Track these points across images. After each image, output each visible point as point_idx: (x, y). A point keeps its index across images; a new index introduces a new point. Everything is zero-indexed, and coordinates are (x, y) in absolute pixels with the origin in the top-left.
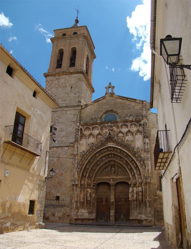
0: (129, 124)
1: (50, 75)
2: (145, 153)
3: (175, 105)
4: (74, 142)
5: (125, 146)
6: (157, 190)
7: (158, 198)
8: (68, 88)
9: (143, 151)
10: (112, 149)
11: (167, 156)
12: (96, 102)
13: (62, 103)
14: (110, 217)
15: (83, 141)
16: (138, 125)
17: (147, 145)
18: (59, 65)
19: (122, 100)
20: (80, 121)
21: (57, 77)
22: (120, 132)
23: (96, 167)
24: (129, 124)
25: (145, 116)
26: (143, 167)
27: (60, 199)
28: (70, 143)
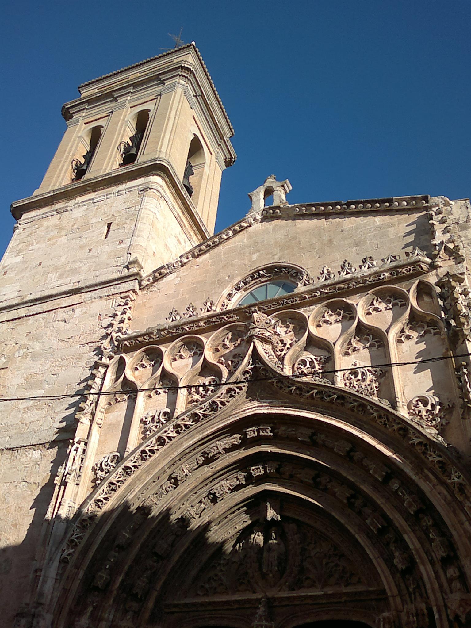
13: (59, 283)
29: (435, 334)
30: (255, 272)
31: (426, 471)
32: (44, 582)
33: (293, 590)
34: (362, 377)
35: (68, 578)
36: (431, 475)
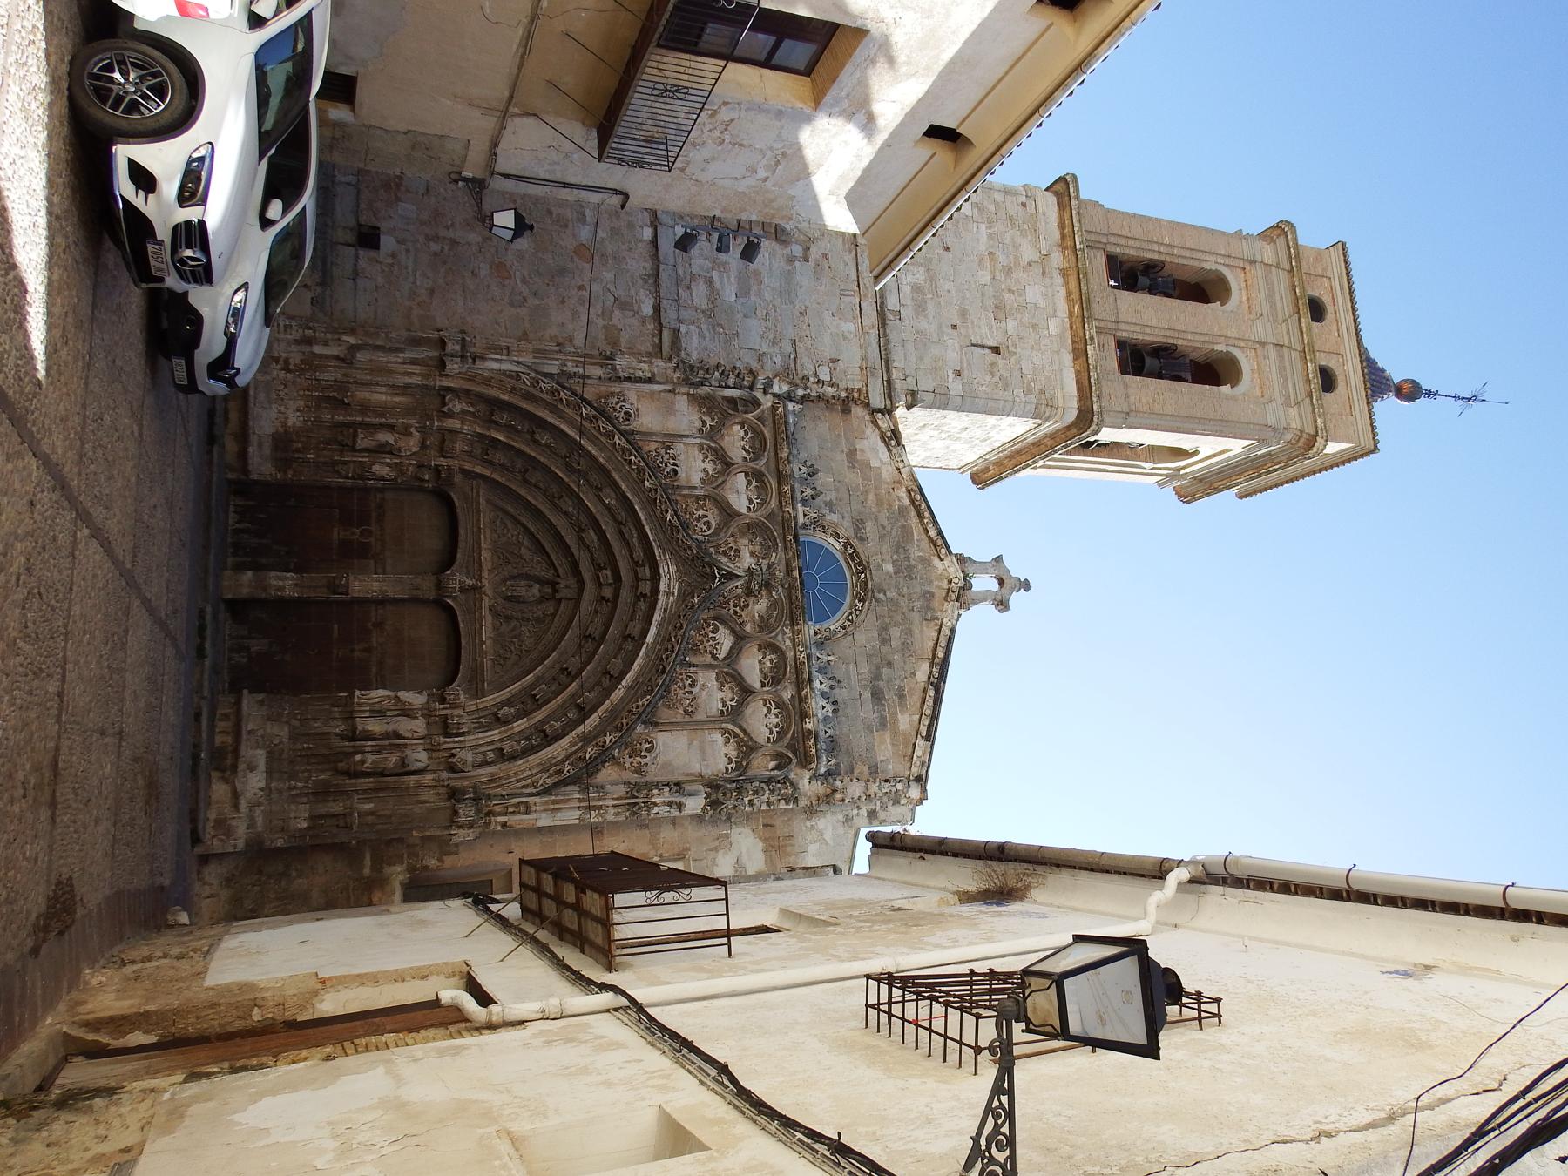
1: (1067, 216)
2: (621, 790)
3: (855, 997)
4: (683, 355)
7: (367, 871)
8: (991, 327)
9: (633, 778)
10: (645, 588)
11: (592, 936)
12: (913, 502)
13: (906, 289)
14: (257, 568)
15: (686, 417)
17: (670, 804)
18: (1134, 274)
20: (803, 397)
21: (1057, 259)
22: (740, 639)
23: (545, 493)
25: (835, 791)
27: (361, 252)
28: (676, 332)
32: (496, 360)
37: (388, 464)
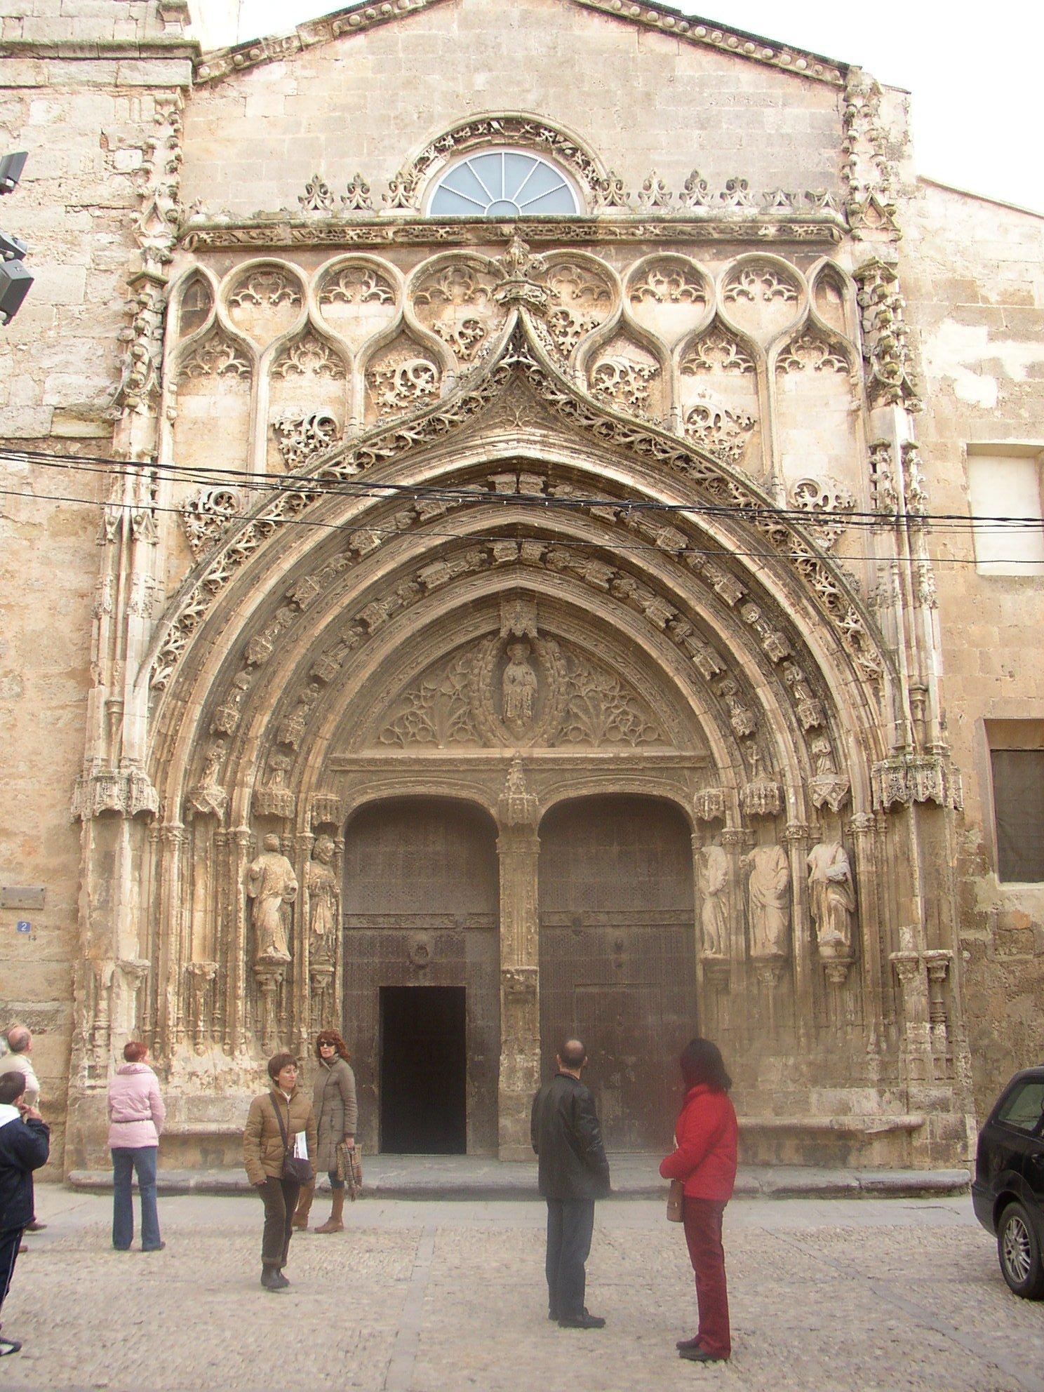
0: (714, 268)
5: (678, 464)
6: (983, 869)
16: (808, 276)
19: (631, 30)
24: (714, 268)
26: (867, 659)
28: (60, 411)
29: (840, 370)
30: (482, 121)
31: (804, 601)
33: (553, 745)
34: (715, 423)
35: (164, 716)
36: (810, 609)
37: (313, 908)
